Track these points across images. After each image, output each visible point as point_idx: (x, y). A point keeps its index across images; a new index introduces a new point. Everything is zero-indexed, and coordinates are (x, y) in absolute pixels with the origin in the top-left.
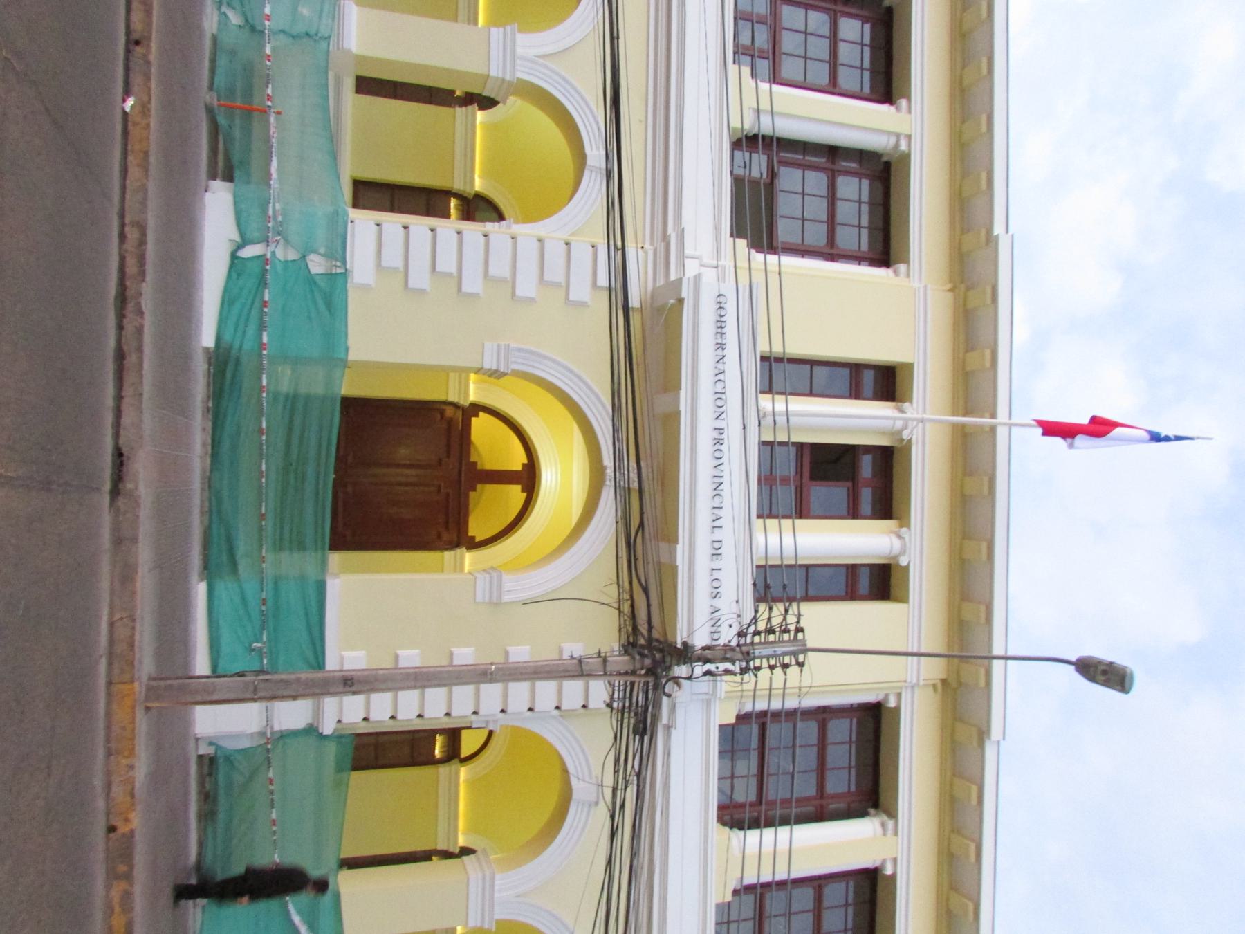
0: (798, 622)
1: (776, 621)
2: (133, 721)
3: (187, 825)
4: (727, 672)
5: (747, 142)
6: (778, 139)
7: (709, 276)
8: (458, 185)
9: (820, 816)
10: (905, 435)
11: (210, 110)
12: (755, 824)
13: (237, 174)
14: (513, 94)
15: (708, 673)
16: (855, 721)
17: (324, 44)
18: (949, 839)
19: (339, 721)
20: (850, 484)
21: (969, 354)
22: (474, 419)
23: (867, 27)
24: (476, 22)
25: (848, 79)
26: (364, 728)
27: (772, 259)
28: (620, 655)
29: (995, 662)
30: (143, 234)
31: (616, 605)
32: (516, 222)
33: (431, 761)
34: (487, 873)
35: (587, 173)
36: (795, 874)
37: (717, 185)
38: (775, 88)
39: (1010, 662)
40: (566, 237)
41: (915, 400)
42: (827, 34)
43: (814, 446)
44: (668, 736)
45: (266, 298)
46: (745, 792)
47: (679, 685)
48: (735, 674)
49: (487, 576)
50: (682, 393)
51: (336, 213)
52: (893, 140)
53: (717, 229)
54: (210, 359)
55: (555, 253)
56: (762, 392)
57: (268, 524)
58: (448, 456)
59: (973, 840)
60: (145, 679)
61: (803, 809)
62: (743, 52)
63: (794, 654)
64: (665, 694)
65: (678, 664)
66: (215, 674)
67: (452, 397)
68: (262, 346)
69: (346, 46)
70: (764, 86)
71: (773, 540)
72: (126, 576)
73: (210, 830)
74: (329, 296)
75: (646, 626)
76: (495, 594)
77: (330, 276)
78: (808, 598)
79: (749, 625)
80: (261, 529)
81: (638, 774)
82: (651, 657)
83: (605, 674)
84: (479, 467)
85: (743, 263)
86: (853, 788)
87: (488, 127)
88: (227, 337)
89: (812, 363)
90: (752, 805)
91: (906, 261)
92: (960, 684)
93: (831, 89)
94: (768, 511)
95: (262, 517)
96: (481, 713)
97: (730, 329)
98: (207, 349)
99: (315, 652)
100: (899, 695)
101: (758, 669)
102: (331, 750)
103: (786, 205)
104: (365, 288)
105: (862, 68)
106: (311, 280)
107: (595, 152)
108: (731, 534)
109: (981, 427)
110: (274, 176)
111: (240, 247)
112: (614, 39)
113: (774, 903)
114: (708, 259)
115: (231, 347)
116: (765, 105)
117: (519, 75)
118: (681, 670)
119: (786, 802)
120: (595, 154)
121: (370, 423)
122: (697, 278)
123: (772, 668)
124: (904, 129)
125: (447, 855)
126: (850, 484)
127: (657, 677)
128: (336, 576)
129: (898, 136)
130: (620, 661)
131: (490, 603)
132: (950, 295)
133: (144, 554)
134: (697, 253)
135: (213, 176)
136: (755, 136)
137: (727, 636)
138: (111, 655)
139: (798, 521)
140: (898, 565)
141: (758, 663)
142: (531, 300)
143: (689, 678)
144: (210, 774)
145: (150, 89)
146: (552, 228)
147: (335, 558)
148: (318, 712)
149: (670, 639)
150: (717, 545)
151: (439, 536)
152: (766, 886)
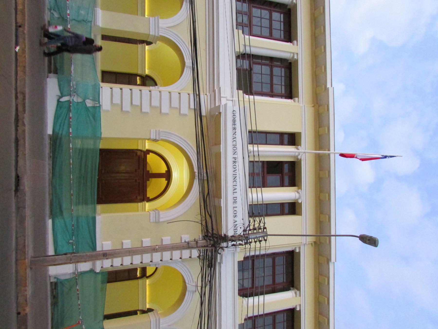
0: (264, 225)
1: (256, 226)
2: (26, 274)
3: (47, 308)
4: (240, 244)
5: (241, 56)
6: (252, 55)
7: (230, 104)
8: (140, 72)
9: (274, 291)
10: (299, 157)
12: (251, 295)
13: (59, 71)
14: (159, 40)
15: (233, 245)
16: (285, 257)
17: (89, 24)
18: (318, 317)
19: (102, 267)
20: (281, 175)
21: (320, 129)
22: (148, 155)
23: (282, 15)
24: (144, 16)
25: (276, 33)
26: (111, 269)
27: (251, 97)
28: (202, 240)
29: (332, 237)
30: (24, 96)
31: (200, 222)
32: (161, 86)
33: (136, 278)
34: (157, 318)
35: (186, 69)
36: (266, 312)
37: (231, 73)
38: (251, 37)
39: (337, 237)
40: (179, 91)
41: (303, 215)
42: (269, 74)
43: (268, 162)
44: (220, 267)
45: (71, 116)
46: (247, 284)
47: (223, 250)
48: (242, 245)
49: (154, 212)
50: (221, 145)
51: (95, 84)
52: (292, 55)
53: (232, 88)
54: (50, 139)
55: (175, 96)
56: (249, 144)
57: (74, 198)
58: (139, 168)
59: (326, 318)
60: (30, 258)
61: (267, 289)
62: (239, 25)
63: (263, 237)
64: (218, 253)
65: (223, 243)
66: (56, 254)
67: (140, 148)
68: (70, 133)
69: (97, 24)
70: (247, 37)
71: (255, 196)
72: (22, 221)
73: (56, 309)
74: (94, 114)
75: (211, 229)
77: (94, 107)
78: (267, 215)
79: (247, 227)
80: (71, 199)
81: (210, 282)
82: (213, 241)
83: (197, 247)
84: (150, 172)
85: (241, 99)
86: (285, 281)
87: (150, 51)
88: (57, 130)
89: (266, 133)
90: (250, 288)
91: (298, 97)
92: (320, 243)
93: (270, 37)
94: (253, 185)
96: (153, 261)
97: (238, 122)
98: (50, 135)
99: (93, 243)
100: (300, 248)
101: (251, 242)
102: (99, 277)
103: (256, 78)
104: (107, 111)
105: (281, 30)
106: (87, 108)
107: (188, 61)
108: (240, 195)
109: (325, 154)
110: (73, 72)
112: (194, 22)
113: (259, 322)
114: (229, 98)
115: (58, 134)
116: (247, 43)
117: (160, 34)
118: (224, 244)
119: (262, 287)
120: (188, 62)
121: (109, 157)
122: (226, 105)
123: (255, 242)
124: (296, 51)
125: (143, 312)
126: (281, 175)
127: (216, 248)
128: (100, 215)
129: (294, 53)
130: (202, 242)
131: (156, 222)
132: (313, 108)
133: (28, 212)
134: (225, 96)
135: (50, 72)
136: (245, 54)
137: (240, 231)
138: (17, 249)
139: (263, 189)
140: (298, 202)
141: (250, 240)
143: (227, 247)
144: (55, 289)
145: (25, 43)
146: (174, 88)
147: (99, 207)
148: (94, 265)
149: (220, 233)
150: (235, 199)
151: (136, 197)
152: (256, 317)
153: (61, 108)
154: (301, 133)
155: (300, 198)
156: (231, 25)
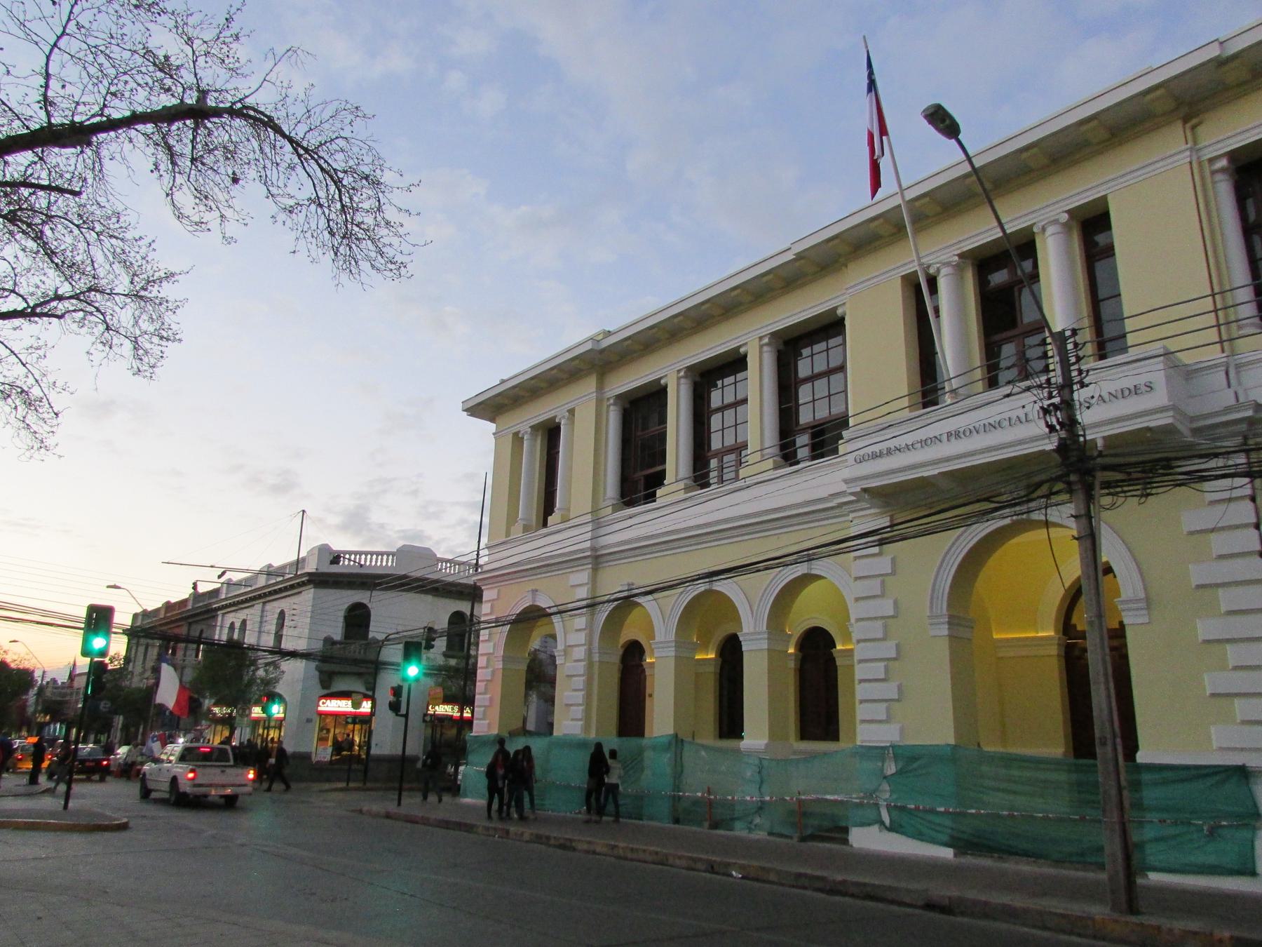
5: (788, 455)
11: (803, 839)
13: (843, 824)
35: (813, 572)
39: (971, 153)
41: (1103, 193)
50: (925, 474)
52: (765, 349)
74: (911, 760)
76: (1140, 605)
95: (1083, 819)
98: (955, 855)
99: (1216, 773)
104: (902, 731)
105: (828, 350)
106: (900, 772)
111: (882, 823)
120: (801, 570)
129: (761, 347)
142: (896, 603)
153: (901, 826)
154: (903, 277)
155: (1056, 222)
156: (794, 476)
